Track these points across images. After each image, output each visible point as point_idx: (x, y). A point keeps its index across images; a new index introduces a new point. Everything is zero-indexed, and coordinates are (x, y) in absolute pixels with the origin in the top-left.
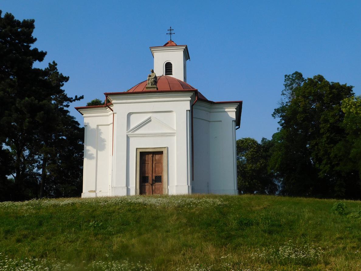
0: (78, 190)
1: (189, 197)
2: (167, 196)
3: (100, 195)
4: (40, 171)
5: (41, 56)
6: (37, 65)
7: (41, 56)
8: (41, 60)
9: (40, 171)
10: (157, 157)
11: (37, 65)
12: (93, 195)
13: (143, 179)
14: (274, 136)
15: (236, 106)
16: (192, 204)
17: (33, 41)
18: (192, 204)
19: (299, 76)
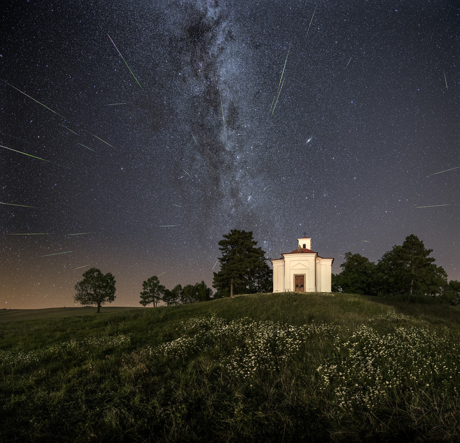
0: (272, 290)
1: (330, 293)
2: (306, 292)
3: (279, 292)
4: (257, 285)
5: (255, 243)
6: (254, 247)
7: (255, 243)
8: (256, 245)
9: (257, 285)
10: (302, 278)
11: (254, 247)
12: (277, 292)
13: (297, 286)
14: (340, 274)
15: (332, 259)
16: (429, 352)
17: (253, 238)
18: (429, 352)
19: (350, 253)
